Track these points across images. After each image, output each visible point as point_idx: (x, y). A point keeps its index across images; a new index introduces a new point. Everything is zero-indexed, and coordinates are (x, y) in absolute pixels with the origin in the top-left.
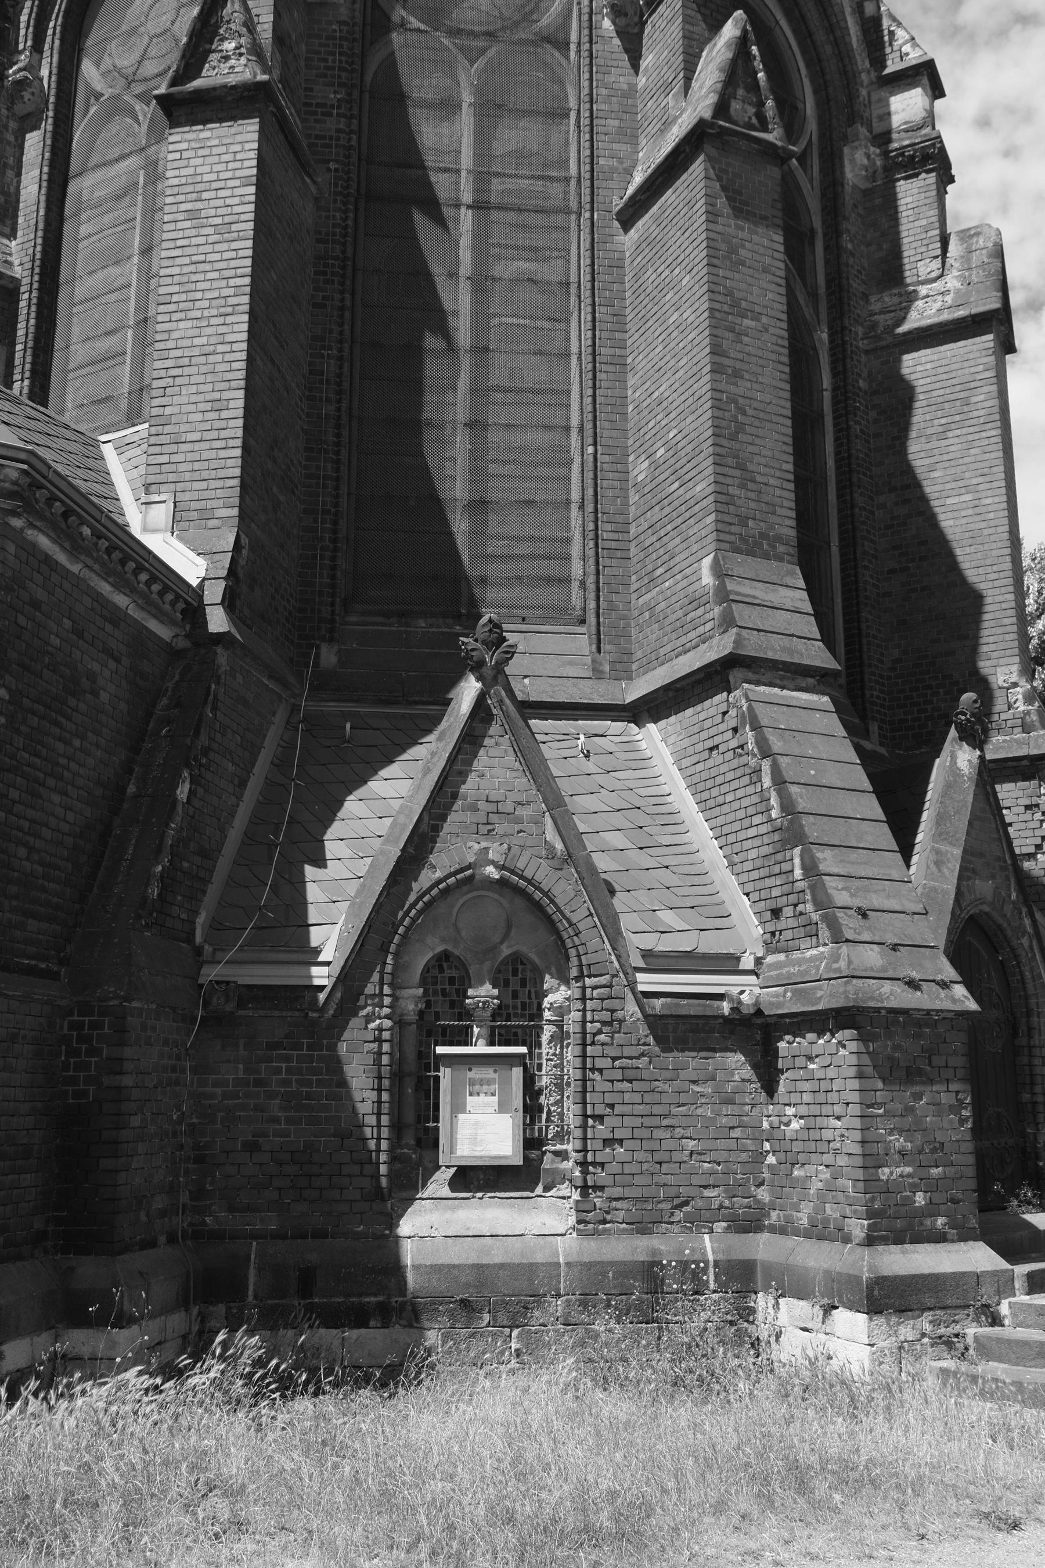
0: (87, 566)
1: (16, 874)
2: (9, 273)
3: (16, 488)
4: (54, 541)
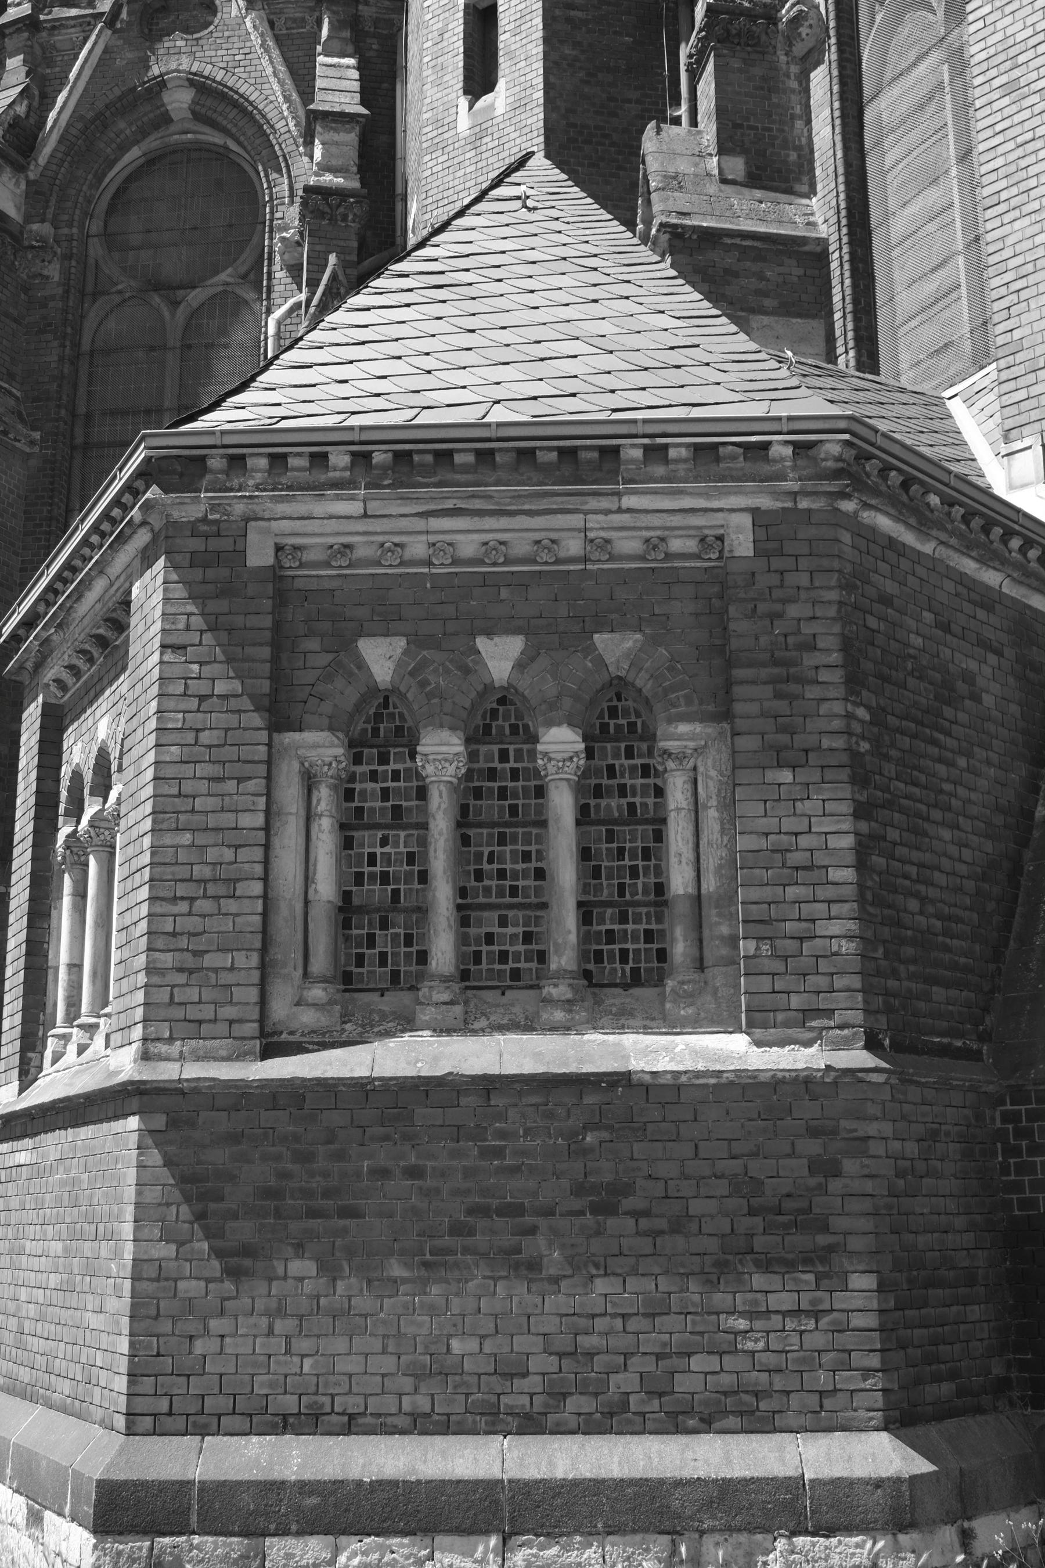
0: (942, 543)
1: (909, 933)
2: (814, 235)
3: (840, 465)
4: (897, 519)
